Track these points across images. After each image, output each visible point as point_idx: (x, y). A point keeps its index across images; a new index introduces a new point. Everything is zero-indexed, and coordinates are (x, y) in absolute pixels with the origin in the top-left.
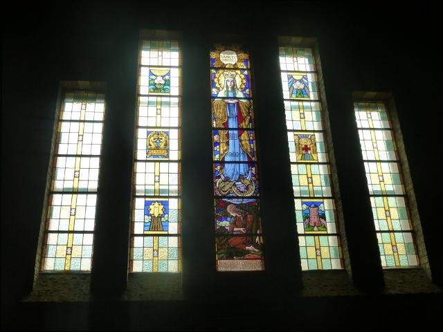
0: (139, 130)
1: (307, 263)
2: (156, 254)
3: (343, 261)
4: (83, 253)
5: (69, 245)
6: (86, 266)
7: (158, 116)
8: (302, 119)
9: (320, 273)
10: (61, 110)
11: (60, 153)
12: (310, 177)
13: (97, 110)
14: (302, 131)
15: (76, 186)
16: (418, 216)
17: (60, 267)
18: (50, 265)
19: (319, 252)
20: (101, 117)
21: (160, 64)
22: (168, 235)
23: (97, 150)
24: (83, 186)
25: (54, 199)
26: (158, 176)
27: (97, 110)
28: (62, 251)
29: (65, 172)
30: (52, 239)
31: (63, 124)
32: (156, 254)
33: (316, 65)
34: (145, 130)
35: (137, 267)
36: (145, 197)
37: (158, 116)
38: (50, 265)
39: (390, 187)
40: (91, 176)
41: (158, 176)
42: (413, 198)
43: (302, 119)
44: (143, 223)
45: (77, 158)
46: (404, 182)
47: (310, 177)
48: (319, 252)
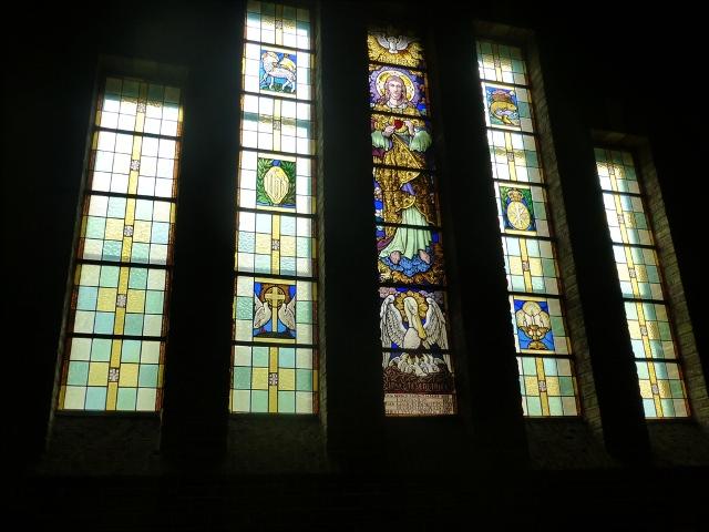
0: (248, 45)
1: (532, 407)
2: (273, 379)
3: (580, 398)
4: (147, 250)
5: (112, 366)
6: (147, 401)
7: (277, 123)
8: (511, 157)
9: (547, 422)
10: (99, 108)
11: (77, 329)
12: (526, 262)
13: (168, 118)
14: (510, 181)
15: (126, 254)
16: (665, 221)
17: (96, 403)
18: (75, 399)
19: (544, 387)
20: (173, 131)
21: (276, 54)
22: (296, 100)
23: (166, 188)
24: (139, 253)
25: (95, 178)
26: (274, 238)
27: (168, 118)
28: (99, 373)
29: (102, 227)
30: (79, 348)
31: (94, 198)
32: (273, 379)
33: (528, 76)
34: (251, 280)
35: (240, 402)
36: (258, 150)
37: (277, 123)
38: (75, 399)
39: (640, 290)
40: (154, 230)
41: (274, 238)
42: (682, 305)
43: (511, 157)
44: (255, 173)
45: (137, 137)
46: (651, 226)
47: (526, 262)
48: (544, 387)
